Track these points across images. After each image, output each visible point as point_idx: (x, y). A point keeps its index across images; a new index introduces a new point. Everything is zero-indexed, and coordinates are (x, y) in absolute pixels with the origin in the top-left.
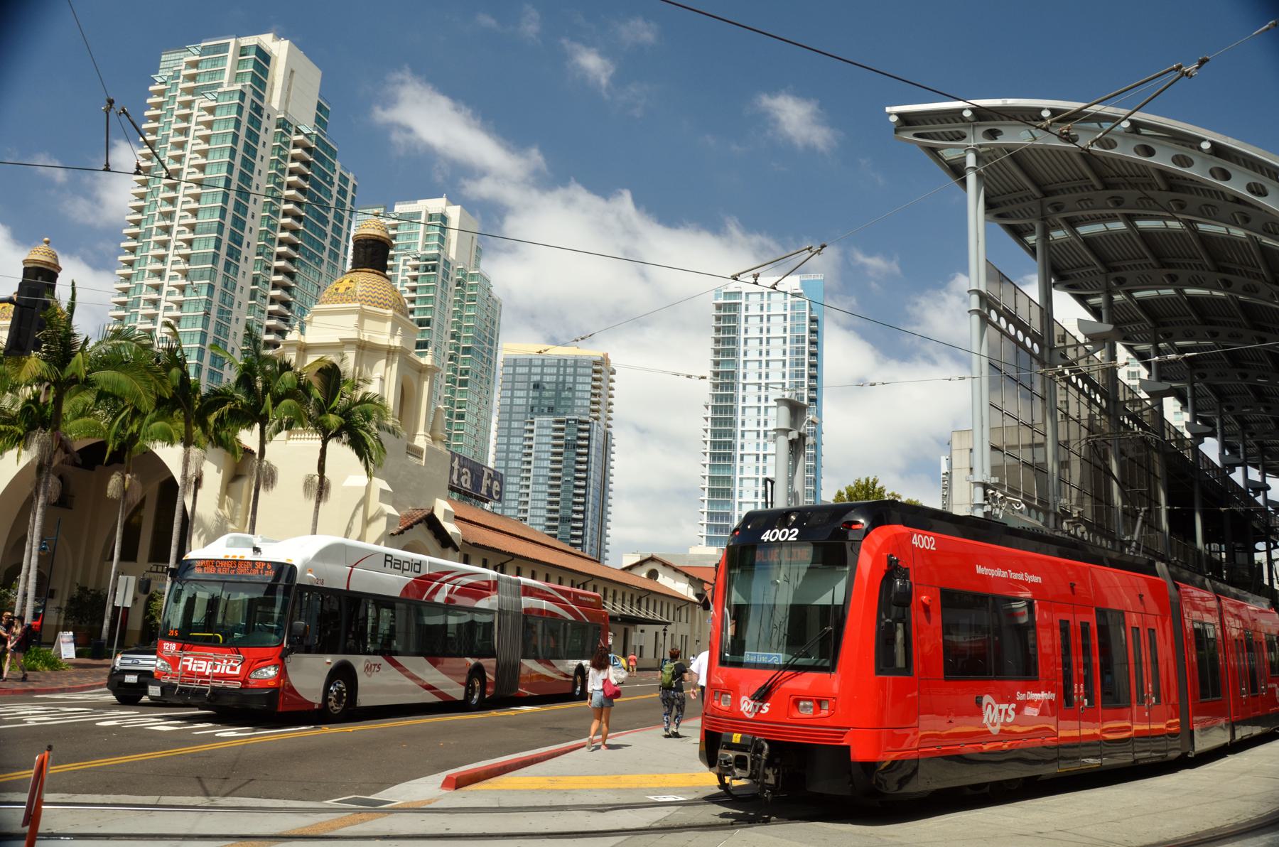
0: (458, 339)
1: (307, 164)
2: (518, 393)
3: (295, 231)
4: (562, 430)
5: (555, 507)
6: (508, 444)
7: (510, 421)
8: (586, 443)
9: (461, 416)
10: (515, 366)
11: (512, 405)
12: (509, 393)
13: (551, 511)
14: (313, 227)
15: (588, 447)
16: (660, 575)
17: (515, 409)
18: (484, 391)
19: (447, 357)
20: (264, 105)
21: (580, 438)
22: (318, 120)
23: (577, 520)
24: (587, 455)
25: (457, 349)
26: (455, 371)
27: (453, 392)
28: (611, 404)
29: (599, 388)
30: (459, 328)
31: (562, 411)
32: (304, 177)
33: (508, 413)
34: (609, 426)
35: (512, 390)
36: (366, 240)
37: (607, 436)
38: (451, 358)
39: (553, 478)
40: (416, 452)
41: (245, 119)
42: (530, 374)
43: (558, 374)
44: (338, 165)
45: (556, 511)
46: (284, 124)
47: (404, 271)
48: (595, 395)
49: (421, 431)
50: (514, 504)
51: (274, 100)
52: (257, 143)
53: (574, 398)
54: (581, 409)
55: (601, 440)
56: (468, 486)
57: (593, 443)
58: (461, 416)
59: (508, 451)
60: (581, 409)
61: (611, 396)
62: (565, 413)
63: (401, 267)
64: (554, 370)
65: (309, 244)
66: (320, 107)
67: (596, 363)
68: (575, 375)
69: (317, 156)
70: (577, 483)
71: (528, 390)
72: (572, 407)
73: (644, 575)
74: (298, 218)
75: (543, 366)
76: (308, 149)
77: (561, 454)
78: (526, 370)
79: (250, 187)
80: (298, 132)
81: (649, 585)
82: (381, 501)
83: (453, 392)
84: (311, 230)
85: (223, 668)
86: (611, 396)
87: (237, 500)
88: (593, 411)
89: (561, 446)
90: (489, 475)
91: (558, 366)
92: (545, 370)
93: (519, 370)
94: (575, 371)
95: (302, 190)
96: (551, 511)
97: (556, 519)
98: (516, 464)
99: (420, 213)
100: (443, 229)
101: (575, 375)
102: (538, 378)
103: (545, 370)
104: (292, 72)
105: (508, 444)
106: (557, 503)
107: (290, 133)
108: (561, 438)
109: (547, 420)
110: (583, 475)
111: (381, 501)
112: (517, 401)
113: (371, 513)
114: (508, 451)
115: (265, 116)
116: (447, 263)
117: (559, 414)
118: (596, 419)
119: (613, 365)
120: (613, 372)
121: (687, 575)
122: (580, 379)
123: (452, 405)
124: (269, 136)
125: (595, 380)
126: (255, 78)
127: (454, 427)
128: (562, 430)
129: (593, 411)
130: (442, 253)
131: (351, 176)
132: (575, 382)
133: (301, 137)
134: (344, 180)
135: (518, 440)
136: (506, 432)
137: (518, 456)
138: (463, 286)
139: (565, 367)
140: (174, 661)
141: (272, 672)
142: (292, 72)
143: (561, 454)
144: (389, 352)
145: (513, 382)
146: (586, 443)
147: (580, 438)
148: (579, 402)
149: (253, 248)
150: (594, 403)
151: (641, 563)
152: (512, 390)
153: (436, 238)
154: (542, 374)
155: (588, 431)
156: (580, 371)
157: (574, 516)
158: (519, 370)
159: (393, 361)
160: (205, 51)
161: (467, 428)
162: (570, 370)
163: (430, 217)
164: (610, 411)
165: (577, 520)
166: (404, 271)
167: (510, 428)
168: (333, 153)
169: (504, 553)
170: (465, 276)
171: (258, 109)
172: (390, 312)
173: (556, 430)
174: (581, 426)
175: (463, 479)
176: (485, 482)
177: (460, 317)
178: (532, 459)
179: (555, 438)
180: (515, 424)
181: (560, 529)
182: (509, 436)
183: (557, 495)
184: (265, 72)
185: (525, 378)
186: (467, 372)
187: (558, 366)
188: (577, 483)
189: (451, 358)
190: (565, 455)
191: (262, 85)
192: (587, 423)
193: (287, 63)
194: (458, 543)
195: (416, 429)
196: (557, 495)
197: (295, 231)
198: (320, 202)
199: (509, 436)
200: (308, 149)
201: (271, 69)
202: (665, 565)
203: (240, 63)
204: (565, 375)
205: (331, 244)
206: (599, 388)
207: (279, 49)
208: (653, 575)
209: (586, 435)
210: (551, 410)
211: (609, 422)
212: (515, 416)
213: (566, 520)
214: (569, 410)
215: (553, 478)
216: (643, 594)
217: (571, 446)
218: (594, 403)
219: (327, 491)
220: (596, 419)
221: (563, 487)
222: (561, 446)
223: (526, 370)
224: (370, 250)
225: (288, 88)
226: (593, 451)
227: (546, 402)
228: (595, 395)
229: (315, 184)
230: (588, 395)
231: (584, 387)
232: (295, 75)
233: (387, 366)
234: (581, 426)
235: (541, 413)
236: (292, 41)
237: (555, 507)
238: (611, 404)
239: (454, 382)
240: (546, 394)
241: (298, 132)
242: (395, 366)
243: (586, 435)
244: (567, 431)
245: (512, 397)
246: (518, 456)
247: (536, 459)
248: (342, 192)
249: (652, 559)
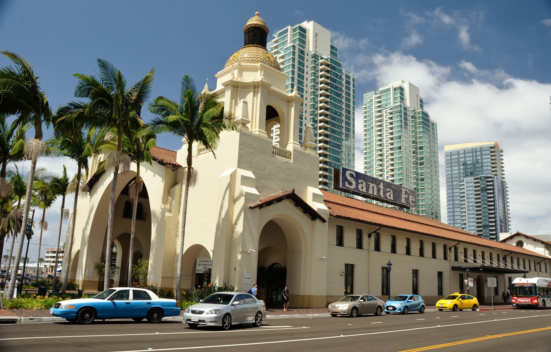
0: (416, 143)
1: (328, 71)
2: (454, 168)
3: (326, 103)
4: (478, 182)
5: (479, 221)
6: (453, 193)
7: (452, 182)
8: (491, 187)
9: (422, 180)
10: (451, 155)
11: (452, 174)
12: (450, 169)
13: (478, 223)
14: (335, 99)
15: (493, 189)
16: (525, 244)
17: (454, 176)
18: (434, 167)
19: (412, 152)
20: (305, 50)
21: (488, 185)
22: (332, 53)
23: (492, 226)
24: (493, 193)
25: (416, 148)
26: (417, 159)
27: (417, 169)
28: (502, 167)
29: (495, 159)
30: (416, 138)
31: (477, 173)
32: (327, 78)
33: (450, 179)
34: (503, 178)
35: (451, 167)
36: (248, 29)
37: (503, 184)
38: (414, 153)
39: (477, 207)
40: (285, 154)
41: (297, 57)
42: (459, 158)
43: (473, 156)
44: (344, 71)
45: (481, 223)
46: (315, 56)
47: (386, 116)
48: (493, 163)
49: (291, 140)
50: (459, 221)
51: (310, 48)
52: (304, 67)
53: (482, 166)
54: (487, 171)
55: (500, 185)
56: (392, 198)
57: (496, 187)
58: (422, 180)
59: (453, 196)
60: (487, 171)
61: (502, 163)
62: (479, 175)
63: (385, 115)
64: (471, 154)
65: (334, 107)
66: (332, 47)
67: (491, 148)
68: (481, 155)
69: (333, 67)
70: (490, 208)
71: (459, 166)
72: (482, 171)
73: (514, 244)
74: (327, 96)
75: (465, 153)
76: (328, 65)
77: (479, 194)
78: (457, 156)
79: (303, 86)
80: (322, 58)
81: (518, 250)
82: (241, 184)
83: (417, 169)
84: (334, 100)
85: (527, 301)
86: (502, 163)
87: (173, 198)
88: (493, 171)
89: (479, 190)
90: (406, 193)
91: (472, 152)
92: (466, 155)
93: (453, 157)
94: (481, 153)
95: (327, 84)
96: (478, 223)
97: (481, 227)
98: (458, 202)
99: (390, 88)
100: (402, 94)
101: (481, 155)
102: (463, 160)
103: (466, 155)
104: (317, 34)
105: (453, 193)
106: (481, 218)
107: (318, 60)
108: (479, 186)
109: (471, 179)
110: (493, 203)
111: (241, 184)
112: (455, 172)
113: (236, 194)
114: (453, 196)
115: (306, 54)
116: (405, 109)
117: (476, 175)
118: (496, 175)
119: (501, 148)
120: (502, 151)
121: (543, 243)
122: (484, 157)
123: (417, 175)
124: (309, 63)
125: (492, 156)
126: (300, 40)
127: (420, 185)
128: (478, 182)
129: (493, 171)
130: (402, 104)
131: (351, 75)
132: (482, 159)
133: (323, 60)
134: (348, 77)
135: (457, 190)
136: (451, 187)
137: (458, 198)
138: (416, 118)
139: (476, 152)
140: (517, 300)
141: (536, 301)
142: (317, 34)
143: (479, 194)
144: (255, 87)
145: (451, 163)
146: (491, 187)
147: (488, 185)
148: (485, 168)
149: (308, 113)
150: (493, 167)
151: (511, 237)
152: (451, 167)
153: (399, 98)
154: (465, 157)
155: (492, 181)
156: (484, 153)
157: (490, 224)
158: (453, 157)
159: (258, 92)
160: (280, 34)
161: (426, 185)
162: (479, 153)
163: (395, 89)
164: (503, 171)
165: (492, 226)
166: (386, 116)
167: (452, 185)
168: (339, 65)
169: (375, 224)
170: (415, 113)
171: (302, 52)
172: (259, 65)
173: (475, 183)
174: (488, 180)
175: (388, 195)
176: (404, 196)
177: (416, 133)
178: (465, 198)
179: (475, 187)
180: (455, 183)
181: (484, 231)
182: (452, 189)
183: (480, 215)
184: (304, 37)
185: (457, 160)
186: (423, 158)
187: (472, 152)
188: (490, 208)
189: (414, 153)
190: (482, 194)
191: (304, 42)
192: (491, 177)
193: (314, 31)
194: (326, 217)
195: (288, 141)
196: (480, 215)
197: (326, 103)
198: (336, 88)
199: (452, 189)
200: (328, 65)
201: (307, 35)
202: (527, 237)
203: (294, 35)
204: (476, 156)
205: (346, 106)
206: (495, 159)
207: (309, 25)
208: (520, 244)
209: (491, 183)
210: (472, 174)
211: (503, 176)
212: (454, 179)
213: (485, 227)
214: (481, 173)
215: (477, 207)
216: (506, 254)
217: (484, 190)
218: (493, 167)
219: (195, 180)
220: (496, 175)
221: (482, 211)
222: (479, 190)
223: (457, 156)
224: (251, 34)
225: (316, 41)
226: (496, 191)
227: (469, 170)
228: (493, 163)
229: (332, 80)
230: (490, 164)
231: (487, 160)
232: (318, 35)
233: (254, 96)
234: (488, 180)
235: (467, 176)
236: (314, 21)
237: (479, 221)
238: (502, 167)
239: (417, 164)
240: (469, 167)
241: (322, 58)
242: (259, 95)
243: (491, 183)
244: (481, 182)
245: (452, 170)
246: (458, 198)
247: (467, 198)
248: (348, 83)
249: (518, 234)
